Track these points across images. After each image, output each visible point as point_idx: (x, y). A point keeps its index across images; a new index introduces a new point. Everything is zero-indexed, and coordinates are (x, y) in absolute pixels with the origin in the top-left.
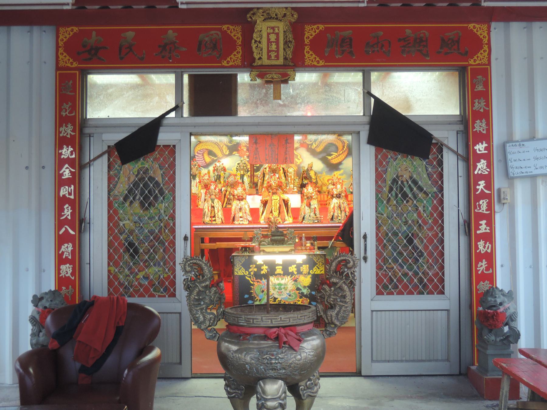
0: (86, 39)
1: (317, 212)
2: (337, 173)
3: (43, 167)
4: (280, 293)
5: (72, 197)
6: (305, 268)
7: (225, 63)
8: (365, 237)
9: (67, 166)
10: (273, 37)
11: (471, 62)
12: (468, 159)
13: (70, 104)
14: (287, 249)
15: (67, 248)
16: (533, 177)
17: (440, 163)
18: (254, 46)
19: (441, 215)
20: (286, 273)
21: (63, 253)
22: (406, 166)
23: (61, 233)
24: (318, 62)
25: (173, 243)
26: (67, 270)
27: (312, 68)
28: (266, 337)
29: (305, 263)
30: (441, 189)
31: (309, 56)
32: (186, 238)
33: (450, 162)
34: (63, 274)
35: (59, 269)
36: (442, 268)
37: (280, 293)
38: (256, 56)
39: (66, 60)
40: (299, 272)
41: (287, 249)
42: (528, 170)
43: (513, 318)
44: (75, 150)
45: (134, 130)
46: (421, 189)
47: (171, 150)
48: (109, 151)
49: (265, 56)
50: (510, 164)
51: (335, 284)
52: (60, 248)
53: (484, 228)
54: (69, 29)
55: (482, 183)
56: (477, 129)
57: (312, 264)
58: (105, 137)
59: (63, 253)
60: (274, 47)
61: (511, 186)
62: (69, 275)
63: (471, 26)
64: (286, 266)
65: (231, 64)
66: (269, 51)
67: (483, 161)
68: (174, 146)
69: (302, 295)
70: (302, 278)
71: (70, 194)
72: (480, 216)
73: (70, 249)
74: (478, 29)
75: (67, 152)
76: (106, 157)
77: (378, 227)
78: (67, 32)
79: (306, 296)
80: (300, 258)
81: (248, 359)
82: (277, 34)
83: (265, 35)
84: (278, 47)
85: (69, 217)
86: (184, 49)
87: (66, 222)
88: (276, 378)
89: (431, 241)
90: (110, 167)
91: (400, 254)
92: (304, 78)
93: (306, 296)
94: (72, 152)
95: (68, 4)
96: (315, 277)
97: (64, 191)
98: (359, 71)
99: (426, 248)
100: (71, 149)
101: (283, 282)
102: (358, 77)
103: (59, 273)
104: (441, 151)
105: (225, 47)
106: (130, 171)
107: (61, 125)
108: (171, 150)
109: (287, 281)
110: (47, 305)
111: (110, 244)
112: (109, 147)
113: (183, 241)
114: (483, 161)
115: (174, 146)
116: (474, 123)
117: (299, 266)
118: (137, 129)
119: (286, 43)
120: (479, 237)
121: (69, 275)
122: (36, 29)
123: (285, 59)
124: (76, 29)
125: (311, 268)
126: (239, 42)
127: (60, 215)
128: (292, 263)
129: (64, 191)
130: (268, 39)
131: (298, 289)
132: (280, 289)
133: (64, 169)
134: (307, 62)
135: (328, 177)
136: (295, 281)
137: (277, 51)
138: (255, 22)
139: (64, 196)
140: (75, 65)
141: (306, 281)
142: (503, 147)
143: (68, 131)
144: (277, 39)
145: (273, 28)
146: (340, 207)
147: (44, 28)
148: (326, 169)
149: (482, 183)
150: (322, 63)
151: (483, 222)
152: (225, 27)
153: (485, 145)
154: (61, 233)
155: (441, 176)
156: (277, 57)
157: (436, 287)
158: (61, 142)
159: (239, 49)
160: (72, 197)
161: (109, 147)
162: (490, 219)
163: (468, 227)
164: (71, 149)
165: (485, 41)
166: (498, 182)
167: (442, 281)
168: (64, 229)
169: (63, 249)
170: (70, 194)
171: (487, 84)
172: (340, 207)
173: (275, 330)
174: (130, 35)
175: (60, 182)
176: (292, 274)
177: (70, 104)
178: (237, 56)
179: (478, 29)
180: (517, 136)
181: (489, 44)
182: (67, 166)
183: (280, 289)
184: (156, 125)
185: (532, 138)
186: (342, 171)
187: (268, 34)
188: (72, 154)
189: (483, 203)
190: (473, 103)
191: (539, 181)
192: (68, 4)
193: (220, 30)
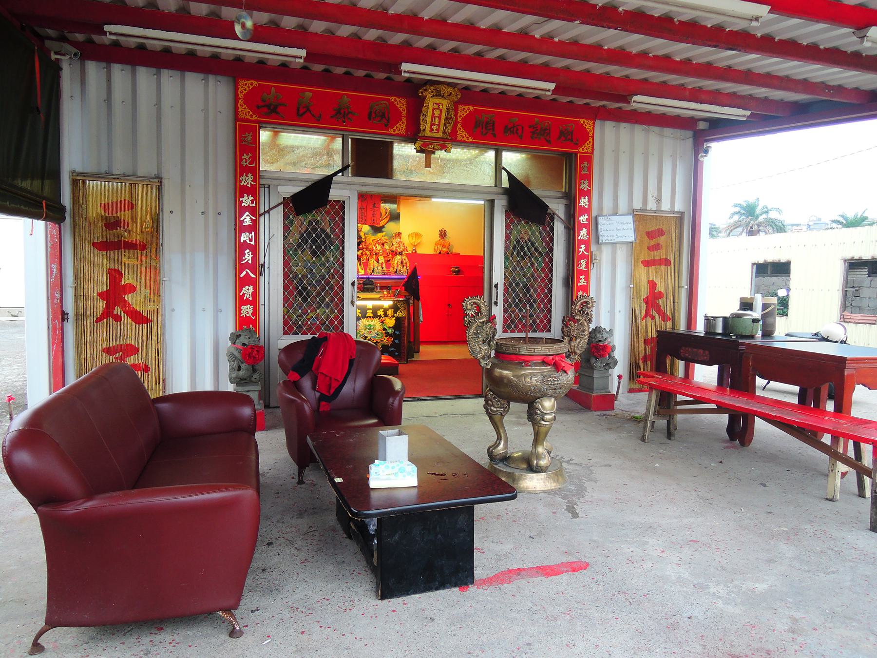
0: (265, 94)
1: (384, 266)
2: (379, 235)
3: (219, 214)
4: (370, 333)
5: (253, 243)
6: (390, 312)
7: (391, 131)
8: (496, 286)
9: (247, 213)
10: (437, 113)
11: (580, 150)
12: (571, 228)
13: (250, 155)
14: (378, 296)
15: (248, 291)
16: (614, 244)
17: (552, 229)
18: (422, 118)
19: (551, 270)
20: (375, 316)
21: (244, 294)
22: (528, 231)
23: (242, 276)
24: (252, 116)
25: (342, 288)
26: (247, 310)
27: (462, 144)
28: (544, 363)
29: (390, 308)
30: (551, 250)
31: (461, 133)
32: (353, 284)
33: (559, 229)
34: (243, 314)
35: (240, 310)
36: (550, 311)
37: (370, 333)
38: (422, 128)
39: (245, 112)
40: (386, 315)
41: (378, 296)
42: (613, 238)
43: (613, 349)
44: (255, 199)
45: (308, 184)
46: (536, 250)
47: (105, 207)
48: (285, 202)
49: (428, 129)
50: (600, 233)
51: (578, 320)
52: (241, 290)
53: (582, 282)
54: (249, 82)
55: (583, 246)
56: (582, 203)
57: (396, 308)
58: (281, 189)
59: (244, 294)
60: (436, 121)
61: (600, 250)
62: (250, 315)
63: (582, 121)
64: (375, 310)
65: (240, 109)
66: (432, 125)
67: (584, 229)
68: (344, 202)
69: (387, 334)
70: (387, 320)
71: (251, 240)
72: (581, 272)
73: (251, 291)
74: (586, 123)
75: (247, 201)
76: (282, 206)
77: (506, 277)
78: (246, 86)
79: (391, 335)
80: (387, 303)
81: (534, 381)
82: (441, 110)
83: (430, 110)
84: (439, 122)
85: (250, 262)
86: (356, 114)
87: (247, 265)
88: (550, 396)
89: (543, 290)
90: (286, 216)
91: (521, 301)
92: (457, 153)
93: (391, 335)
94: (252, 201)
95: (301, 58)
96: (398, 319)
97: (244, 237)
98: (492, 149)
99: (539, 296)
100: (251, 198)
101: (372, 323)
102: (491, 154)
103: (240, 314)
104: (552, 219)
105: (388, 118)
106: (302, 222)
107: (241, 175)
108: (105, 207)
109: (376, 322)
110: (246, 342)
111: (285, 287)
112: (284, 198)
113: (350, 286)
114: (584, 229)
115: (344, 202)
116: (580, 199)
117: (385, 310)
118: (310, 184)
119: (446, 119)
120: (580, 288)
121: (250, 315)
122: (211, 78)
123: (444, 132)
124: (255, 83)
125: (395, 312)
126: (404, 113)
127: (241, 260)
128: (379, 308)
129: (244, 237)
130: (433, 114)
131: (384, 329)
132: (370, 329)
133: (244, 217)
134: (590, 150)
135: (373, 238)
136: (382, 322)
137: (439, 125)
138: (425, 98)
139: (245, 241)
140: (255, 118)
141: (391, 322)
142: (596, 218)
143: (247, 180)
144: (440, 115)
145: (438, 104)
146: (402, 262)
147: (219, 78)
148: (372, 231)
149: (583, 246)
150: (470, 140)
151: (582, 277)
152: (392, 99)
153: (586, 217)
154: (242, 276)
155: (552, 240)
156: (438, 130)
157: (545, 327)
158: (243, 190)
159: (404, 120)
160: (253, 243)
161: (284, 198)
162: (587, 274)
163: (569, 281)
164: (251, 198)
165: (591, 134)
166: (593, 248)
167: (549, 321)
168: (244, 273)
169: (244, 290)
170: (251, 240)
171: (590, 169)
172: (402, 262)
173: (551, 357)
174: (309, 95)
175: (240, 228)
176: (380, 316)
177: (250, 155)
178: (401, 127)
179: (586, 123)
180: (605, 213)
181: (593, 137)
182: (247, 213)
183: (370, 329)
184: (325, 183)
185: (615, 214)
186: (384, 234)
187: (434, 109)
188: (252, 203)
189: (583, 262)
190: (580, 183)
191: (618, 246)
192: (301, 58)
193: (388, 100)
